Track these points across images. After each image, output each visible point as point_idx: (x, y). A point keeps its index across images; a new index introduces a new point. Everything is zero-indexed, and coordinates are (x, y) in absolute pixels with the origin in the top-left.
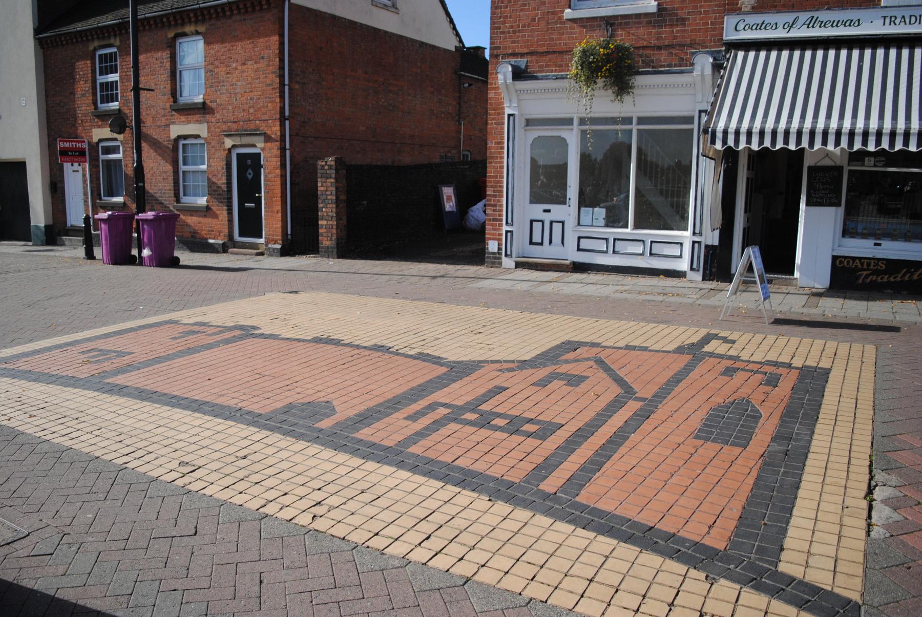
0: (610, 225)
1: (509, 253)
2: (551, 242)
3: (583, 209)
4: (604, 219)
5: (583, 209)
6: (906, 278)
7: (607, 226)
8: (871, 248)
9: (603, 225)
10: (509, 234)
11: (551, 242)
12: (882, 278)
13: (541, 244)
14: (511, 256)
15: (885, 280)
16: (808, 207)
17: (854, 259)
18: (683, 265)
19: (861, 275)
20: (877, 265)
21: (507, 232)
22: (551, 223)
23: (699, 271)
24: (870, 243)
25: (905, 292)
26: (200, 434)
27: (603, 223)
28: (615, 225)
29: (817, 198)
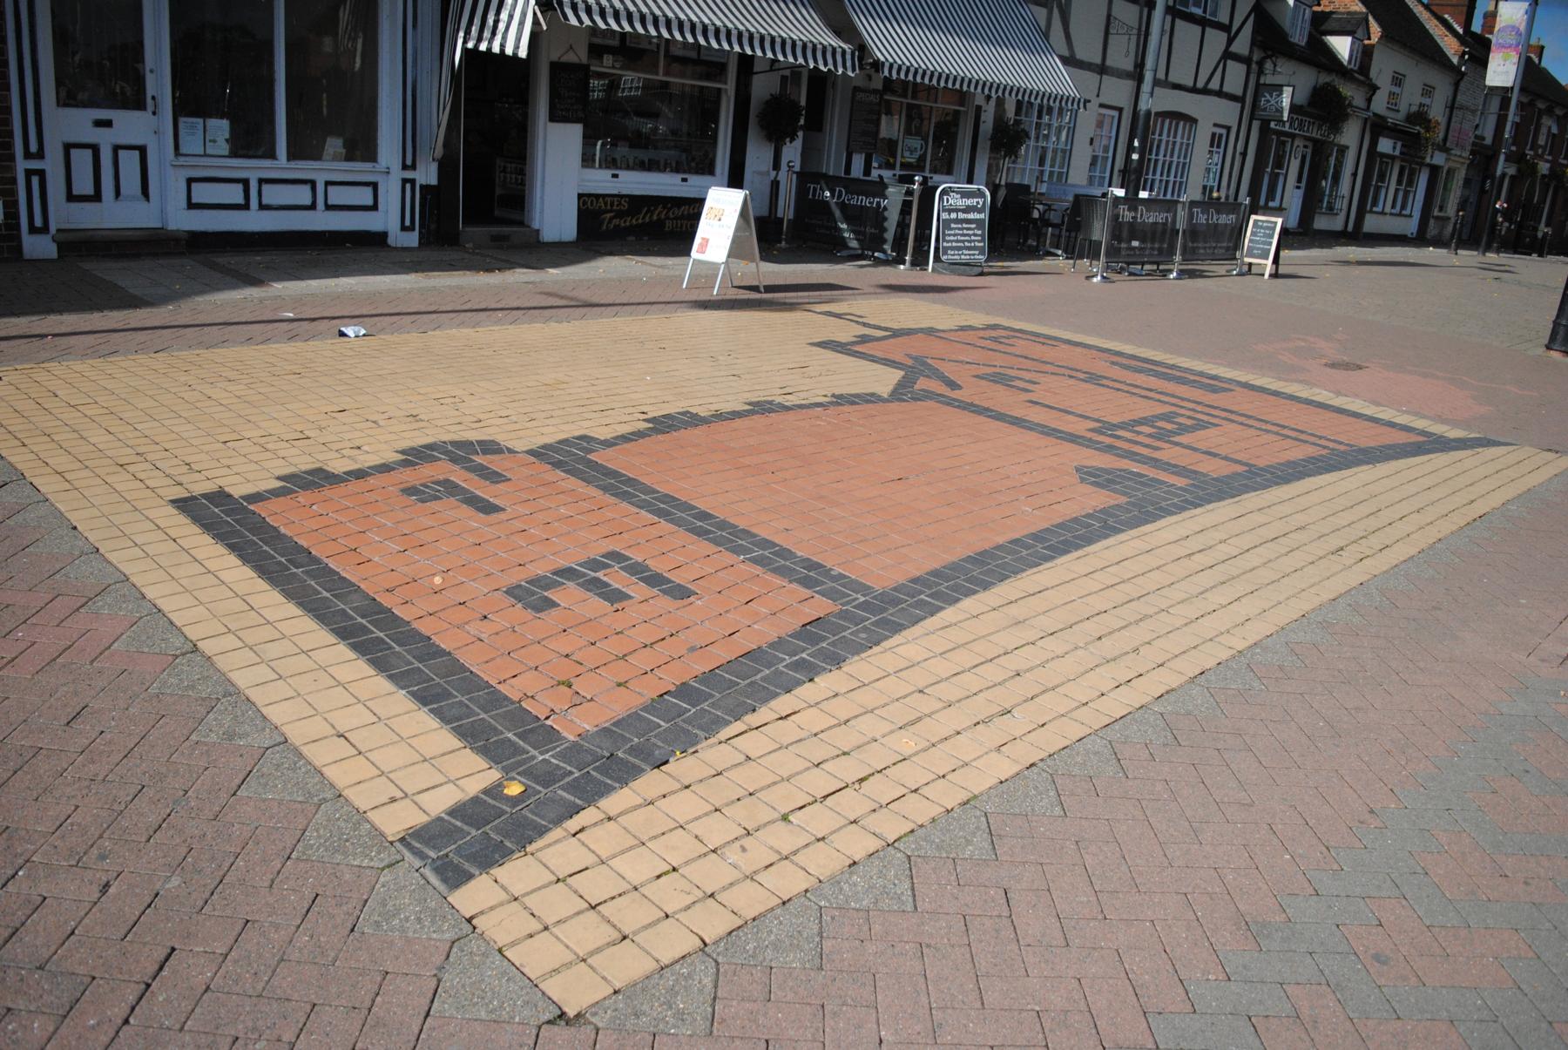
0: (241, 152)
1: (38, 222)
2: (118, 193)
3: (182, 120)
4: (227, 140)
5: (182, 120)
6: (647, 220)
7: (234, 154)
8: (607, 182)
9: (227, 154)
10: (35, 180)
11: (118, 193)
12: (625, 222)
13: (97, 197)
14: (45, 229)
15: (628, 224)
16: (975, 181)
17: (597, 196)
18: (387, 219)
19: (604, 219)
20: (620, 204)
21: (29, 173)
22: (116, 149)
23: (413, 229)
24: (676, 179)
25: (646, 238)
26: (1170, 610)
27: (224, 149)
28: (251, 153)
29: (562, 110)
